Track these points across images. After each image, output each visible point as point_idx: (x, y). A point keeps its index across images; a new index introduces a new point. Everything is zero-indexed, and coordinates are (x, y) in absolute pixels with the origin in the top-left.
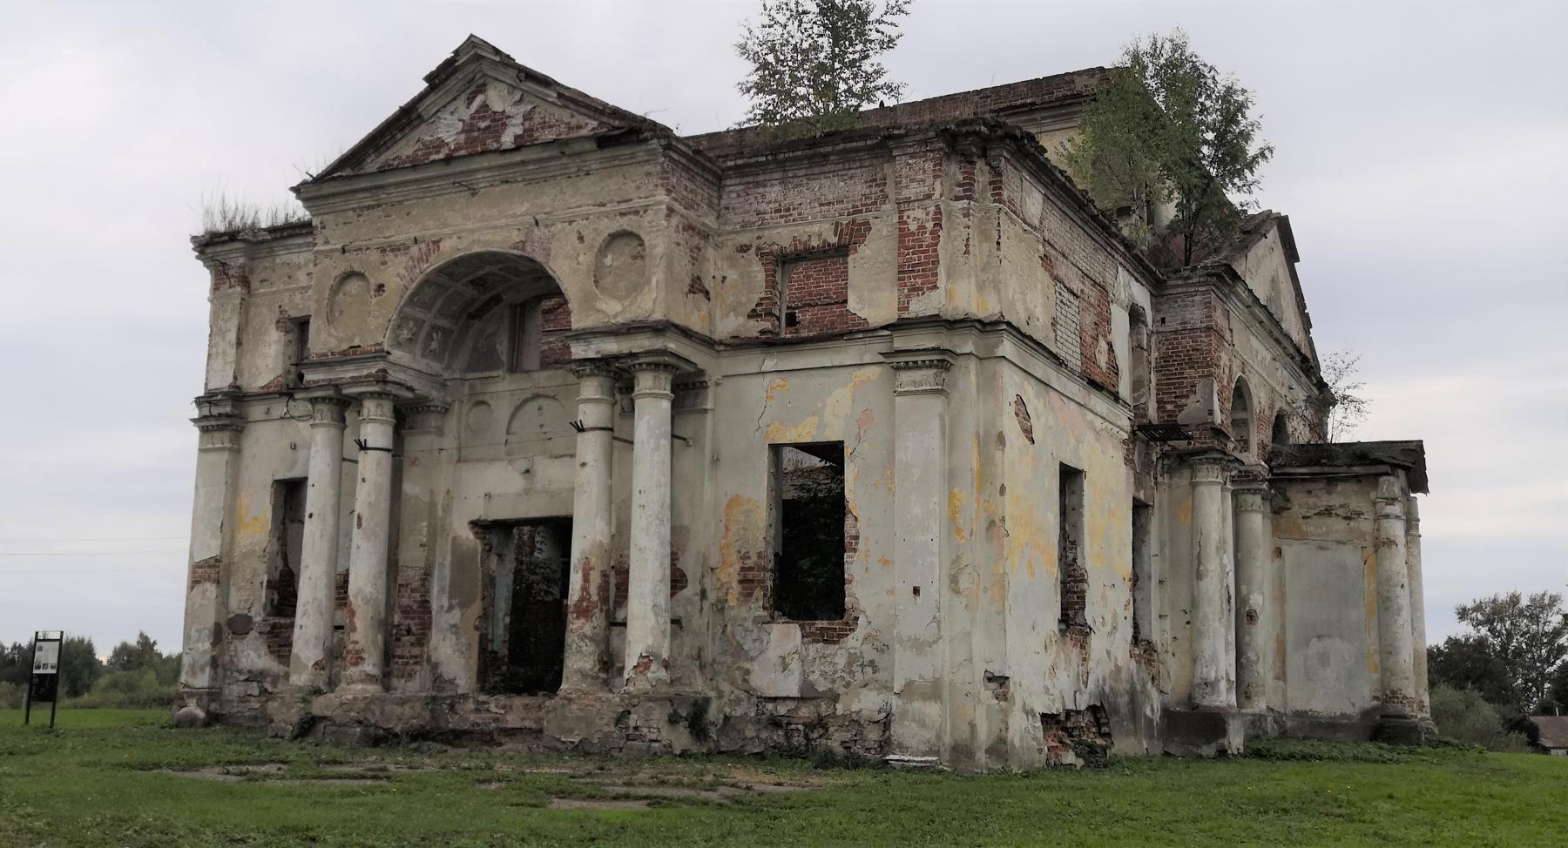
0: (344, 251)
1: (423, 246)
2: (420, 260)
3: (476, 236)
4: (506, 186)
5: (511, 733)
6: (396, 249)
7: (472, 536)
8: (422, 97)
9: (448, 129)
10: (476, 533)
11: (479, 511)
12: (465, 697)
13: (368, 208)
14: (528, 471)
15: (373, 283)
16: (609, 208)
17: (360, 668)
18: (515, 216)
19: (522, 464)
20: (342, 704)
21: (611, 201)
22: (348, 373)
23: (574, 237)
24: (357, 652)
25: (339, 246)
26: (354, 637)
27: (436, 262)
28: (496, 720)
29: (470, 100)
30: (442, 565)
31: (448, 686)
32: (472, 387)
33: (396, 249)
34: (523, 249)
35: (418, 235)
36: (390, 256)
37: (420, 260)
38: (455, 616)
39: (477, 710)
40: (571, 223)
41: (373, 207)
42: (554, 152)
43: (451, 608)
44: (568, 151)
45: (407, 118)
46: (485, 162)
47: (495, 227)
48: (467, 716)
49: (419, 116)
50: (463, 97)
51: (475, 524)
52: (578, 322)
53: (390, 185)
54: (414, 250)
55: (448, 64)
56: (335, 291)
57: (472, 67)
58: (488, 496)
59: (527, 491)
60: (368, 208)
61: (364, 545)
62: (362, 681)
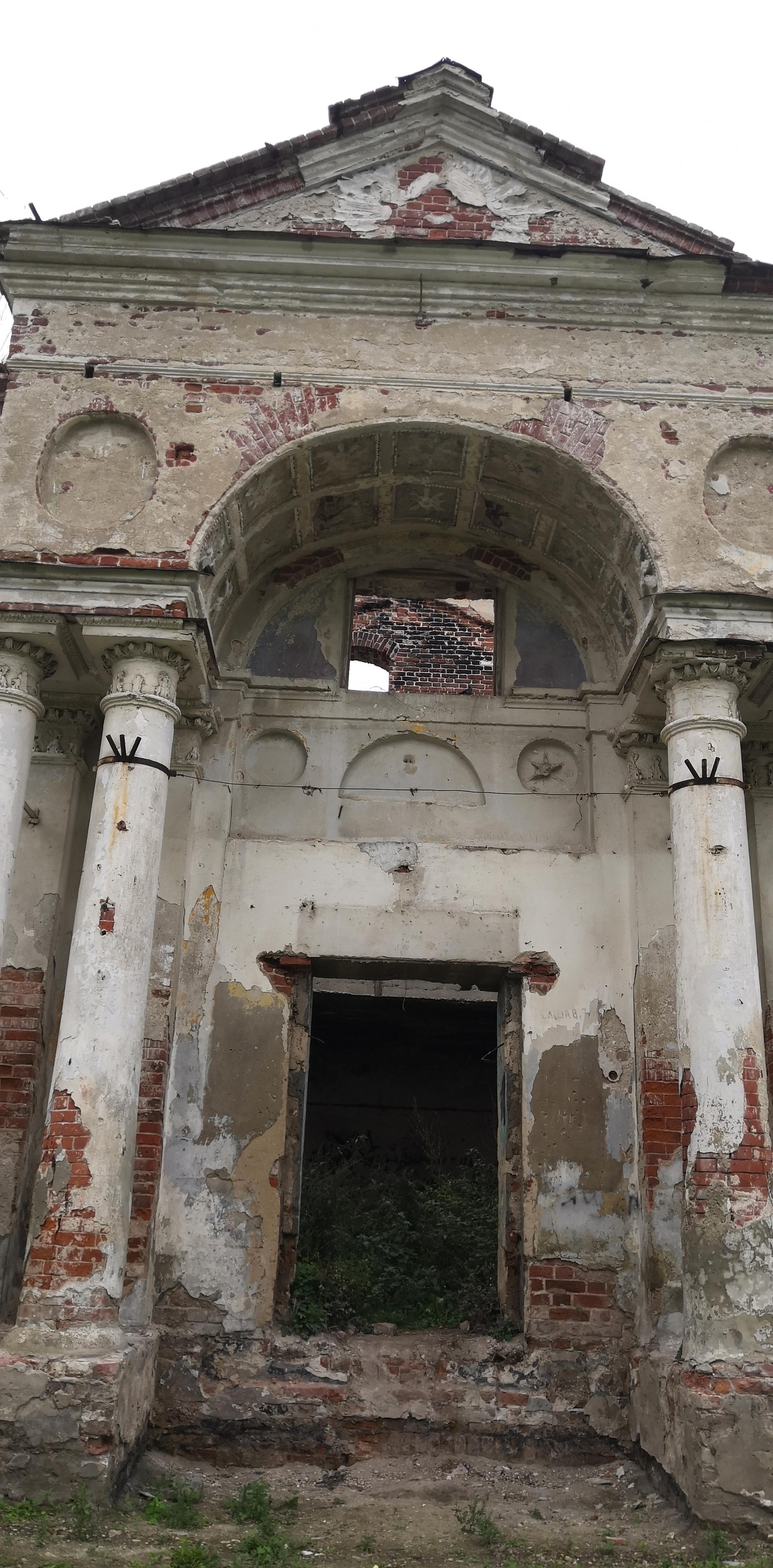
0: (89, 372)
1: (297, 394)
2: (288, 414)
3: (426, 394)
4: (496, 323)
5: (376, 1431)
6: (225, 388)
7: (266, 985)
8: (315, 141)
9: (365, 206)
10: (274, 980)
11: (287, 936)
12: (241, 1339)
13: (160, 306)
14: (404, 868)
15: (164, 441)
16: (730, 393)
17: (94, 1282)
18: (522, 375)
19: (393, 856)
20: (53, 1386)
21: (738, 385)
22: (90, 598)
23: (655, 431)
24: (90, 1238)
25: (83, 361)
26: (81, 1198)
27: (325, 424)
28: (332, 1397)
29: (406, 178)
30: (190, 1040)
31: (193, 1311)
32: (259, 701)
33: (225, 388)
34: (536, 433)
35: (285, 370)
36: (210, 400)
37: (288, 414)
38: (222, 1153)
39: (275, 1372)
40: (645, 406)
41: (173, 306)
42: (630, 275)
43: (209, 1134)
44: (659, 280)
45: (270, 169)
46: (475, 264)
47: (474, 386)
48: (247, 1384)
49: (298, 176)
50: (392, 170)
51: (269, 961)
52: (667, 579)
53: (231, 270)
54: (274, 397)
55: (385, 96)
56: (57, 443)
57: (424, 121)
58: (309, 908)
59: (403, 907)
60: (160, 306)
61: (118, 975)
62: (95, 1317)
